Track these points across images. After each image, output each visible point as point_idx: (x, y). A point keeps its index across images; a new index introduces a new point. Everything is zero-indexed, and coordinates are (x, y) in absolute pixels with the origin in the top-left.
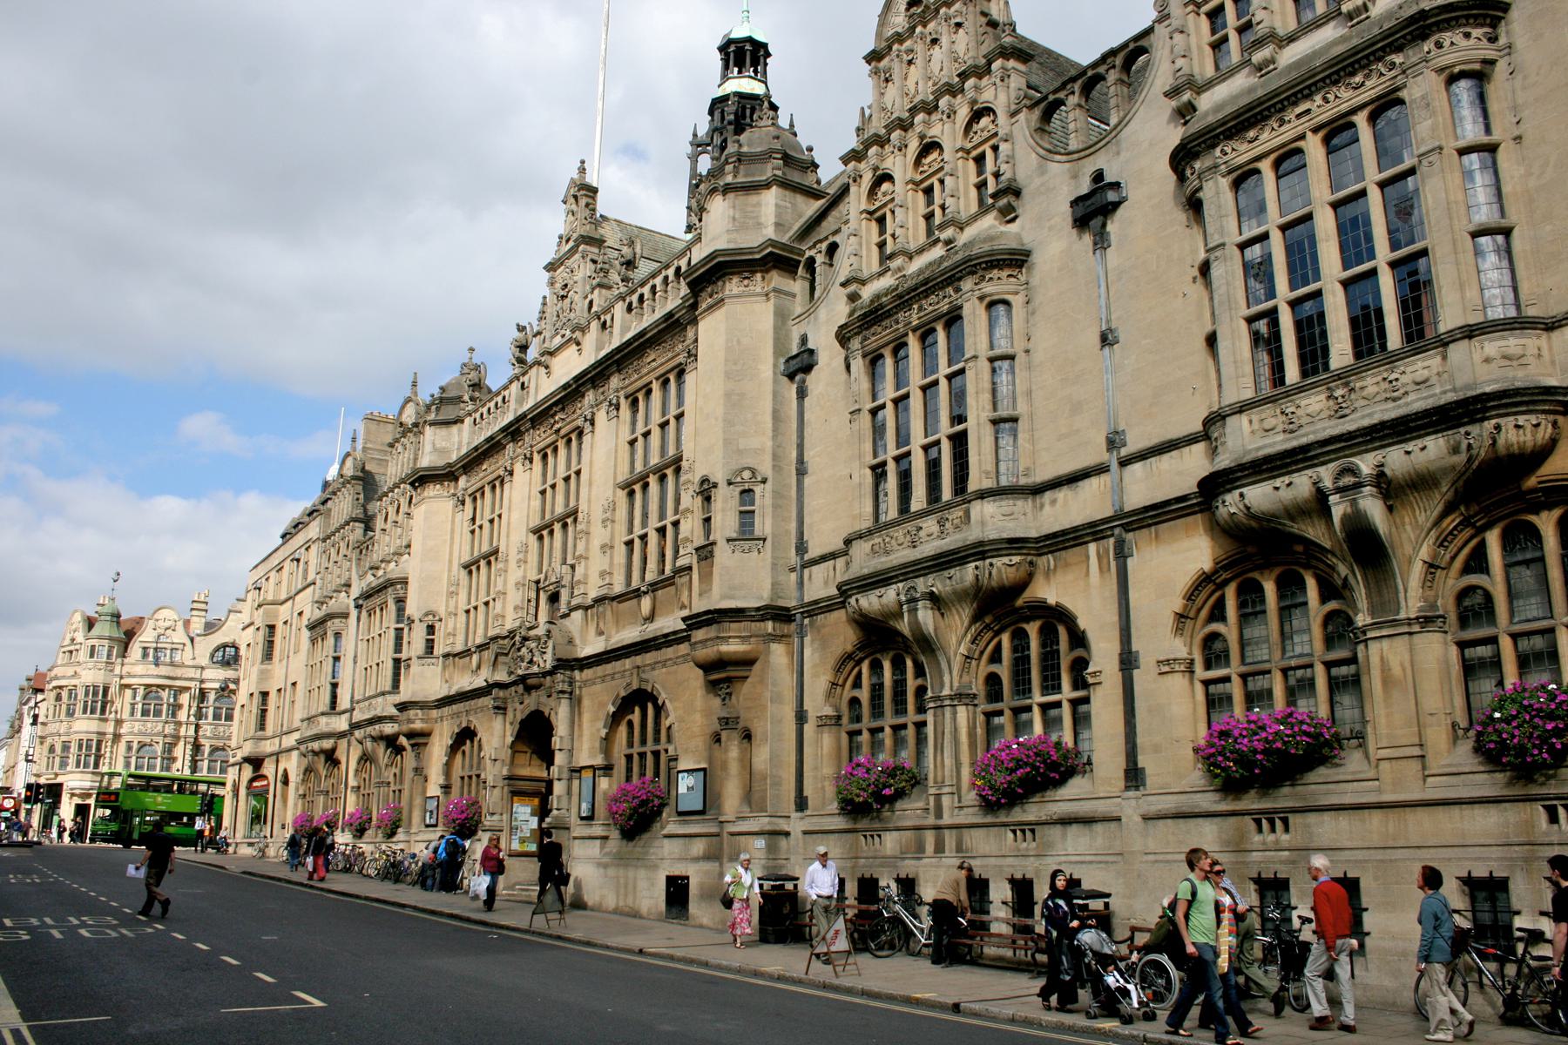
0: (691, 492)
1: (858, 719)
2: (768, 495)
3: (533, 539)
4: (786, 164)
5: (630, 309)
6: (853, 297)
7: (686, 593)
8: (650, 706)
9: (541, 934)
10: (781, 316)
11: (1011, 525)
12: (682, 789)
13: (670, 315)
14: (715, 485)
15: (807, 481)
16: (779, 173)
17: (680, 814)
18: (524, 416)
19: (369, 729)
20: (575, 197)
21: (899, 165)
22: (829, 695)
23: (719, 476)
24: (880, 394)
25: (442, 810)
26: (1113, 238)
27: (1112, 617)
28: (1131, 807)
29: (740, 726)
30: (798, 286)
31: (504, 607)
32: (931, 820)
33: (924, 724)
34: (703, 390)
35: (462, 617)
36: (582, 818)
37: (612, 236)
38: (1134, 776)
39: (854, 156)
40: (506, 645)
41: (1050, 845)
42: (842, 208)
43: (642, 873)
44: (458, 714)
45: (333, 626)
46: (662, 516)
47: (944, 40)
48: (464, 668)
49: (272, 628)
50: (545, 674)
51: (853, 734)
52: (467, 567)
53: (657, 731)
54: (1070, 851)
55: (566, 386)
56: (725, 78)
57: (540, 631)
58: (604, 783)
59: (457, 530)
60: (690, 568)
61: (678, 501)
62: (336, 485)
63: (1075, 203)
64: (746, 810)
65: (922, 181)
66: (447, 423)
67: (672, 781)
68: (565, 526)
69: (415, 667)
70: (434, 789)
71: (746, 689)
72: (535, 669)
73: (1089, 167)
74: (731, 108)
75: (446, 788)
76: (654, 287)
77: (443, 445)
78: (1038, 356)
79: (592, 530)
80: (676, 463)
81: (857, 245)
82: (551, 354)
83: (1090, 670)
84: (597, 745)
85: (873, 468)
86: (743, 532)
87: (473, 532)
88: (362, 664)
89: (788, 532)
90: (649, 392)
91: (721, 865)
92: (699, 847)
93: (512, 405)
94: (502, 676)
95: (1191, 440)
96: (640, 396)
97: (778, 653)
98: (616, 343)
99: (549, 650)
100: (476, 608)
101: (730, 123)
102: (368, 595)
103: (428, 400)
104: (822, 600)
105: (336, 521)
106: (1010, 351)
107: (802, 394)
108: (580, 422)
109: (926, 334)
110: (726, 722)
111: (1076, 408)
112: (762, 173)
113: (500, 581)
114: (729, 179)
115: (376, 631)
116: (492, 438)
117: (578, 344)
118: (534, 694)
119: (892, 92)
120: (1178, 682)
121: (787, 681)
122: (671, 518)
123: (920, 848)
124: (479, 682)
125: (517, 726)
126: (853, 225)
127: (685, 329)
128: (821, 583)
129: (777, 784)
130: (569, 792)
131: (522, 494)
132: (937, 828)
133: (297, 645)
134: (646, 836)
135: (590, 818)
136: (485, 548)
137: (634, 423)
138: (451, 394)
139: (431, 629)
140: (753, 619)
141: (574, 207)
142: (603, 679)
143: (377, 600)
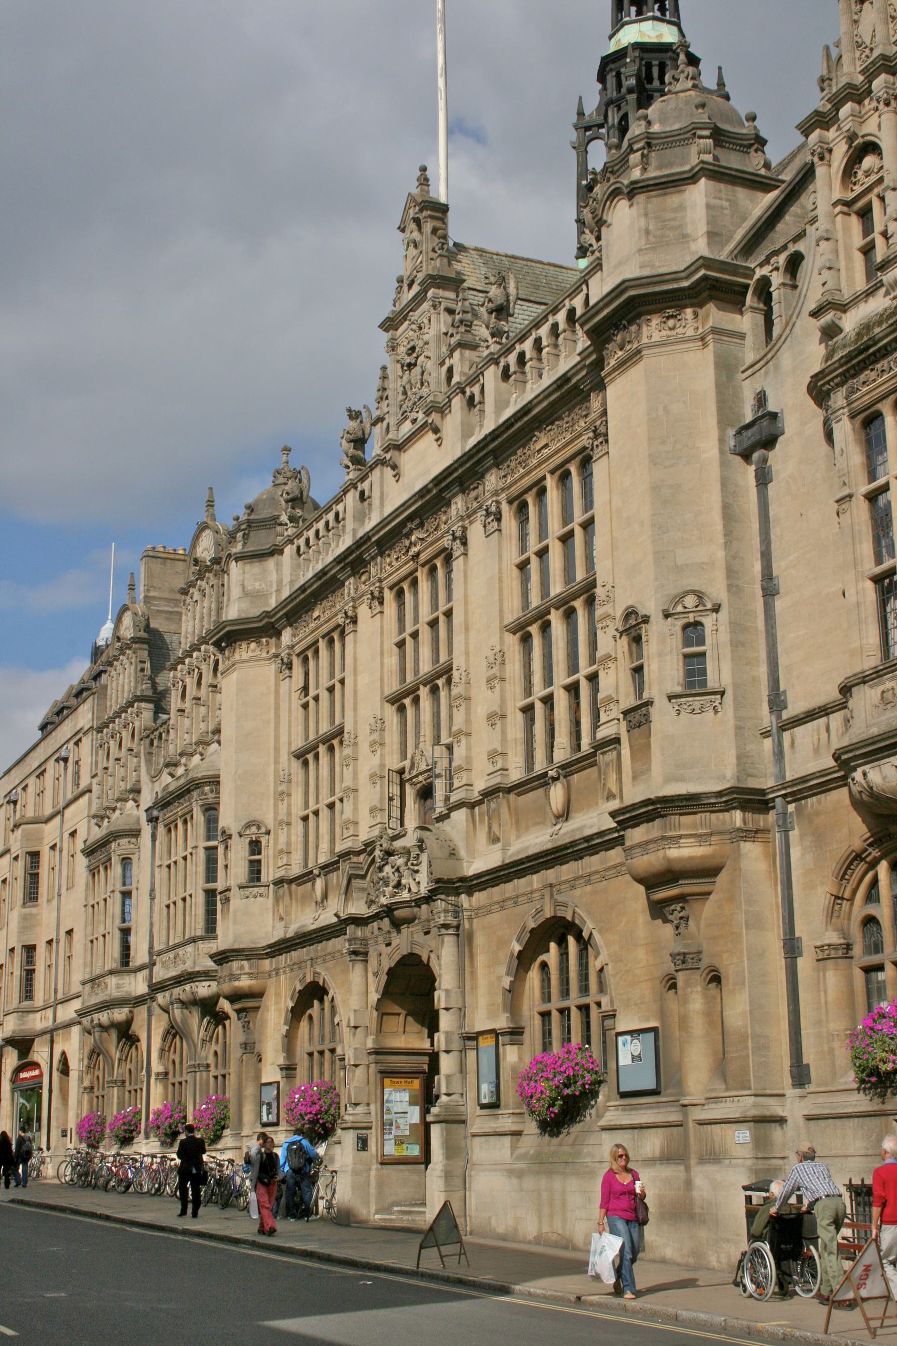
0: (611, 631)
1: (877, 948)
2: (724, 629)
3: (390, 711)
4: (718, 143)
5: (506, 375)
6: (830, 332)
7: (613, 777)
8: (571, 940)
9: (433, 1277)
10: (726, 369)
12: (625, 1059)
13: (564, 379)
14: (646, 620)
15: (779, 604)
16: (708, 158)
17: (624, 1095)
18: (366, 538)
19: (177, 991)
20: (417, 221)
22: (831, 914)
23: (651, 606)
24: (880, 469)
25: (284, 1101)
29: (703, 964)
30: (747, 322)
34: (618, 481)
35: (299, 827)
36: (483, 1107)
37: (472, 272)
39: (821, 120)
40: (359, 863)
42: (806, 200)
43: (573, 1184)
44: (300, 964)
45: (119, 848)
46: (573, 668)
48: (305, 899)
49: (35, 856)
50: (419, 902)
52: (301, 756)
53: (584, 977)
55: (422, 492)
57: (409, 841)
58: (511, 1055)
59: (284, 706)
60: (617, 740)
62: (112, 652)
64: (720, 1089)
66: (260, 556)
67: (609, 1048)
68: (435, 690)
69: (236, 901)
70: (271, 1073)
71: (708, 909)
72: (405, 895)
74: (630, 69)
75: (289, 1069)
76: (538, 341)
79: (474, 693)
80: (589, 591)
81: (832, 252)
82: (400, 447)
84: (499, 1000)
85: (877, 580)
86: (690, 685)
87: (305, 706)
88: (162, 900)
89: (755, 680)
90: (542, 492)
91: (688, 1169)
93: (349, 524)
94: (358, 908)
96: (530, 499)
97: (751, 850)
98: (489, 426)
99: (424, 868)
100: (316, 813)
101: (630, 91)
102: (164, 803)
103: (231, 524)
104: (812, 776)
105: (115, 700)
107: (763, 479)
108: (446, 542)
110: (684, 960)
112: (684, 160)
113: (348, 773)
114: (636, 174)
115: (178, 853)
116: (323, 573)
117: (436, 430)
118: (404, 929)
121: (769, 897)
122: (585, 669)
124: (327, 918)
126: (823, 224)
127: (587, 398)
128: (809, 751)
129: (763, 1046)
130: (462, 1069)
131: (371, 652)
133: (71, 878)
134: (576, 1128)
135: (495, 1105)
136: (325, 728)
137: (523, 537)
138: (264, 513)
139: (255, 846)
140: (713, 809)
141: (416, 235)
142: (502, 904)
143: (177, 809)
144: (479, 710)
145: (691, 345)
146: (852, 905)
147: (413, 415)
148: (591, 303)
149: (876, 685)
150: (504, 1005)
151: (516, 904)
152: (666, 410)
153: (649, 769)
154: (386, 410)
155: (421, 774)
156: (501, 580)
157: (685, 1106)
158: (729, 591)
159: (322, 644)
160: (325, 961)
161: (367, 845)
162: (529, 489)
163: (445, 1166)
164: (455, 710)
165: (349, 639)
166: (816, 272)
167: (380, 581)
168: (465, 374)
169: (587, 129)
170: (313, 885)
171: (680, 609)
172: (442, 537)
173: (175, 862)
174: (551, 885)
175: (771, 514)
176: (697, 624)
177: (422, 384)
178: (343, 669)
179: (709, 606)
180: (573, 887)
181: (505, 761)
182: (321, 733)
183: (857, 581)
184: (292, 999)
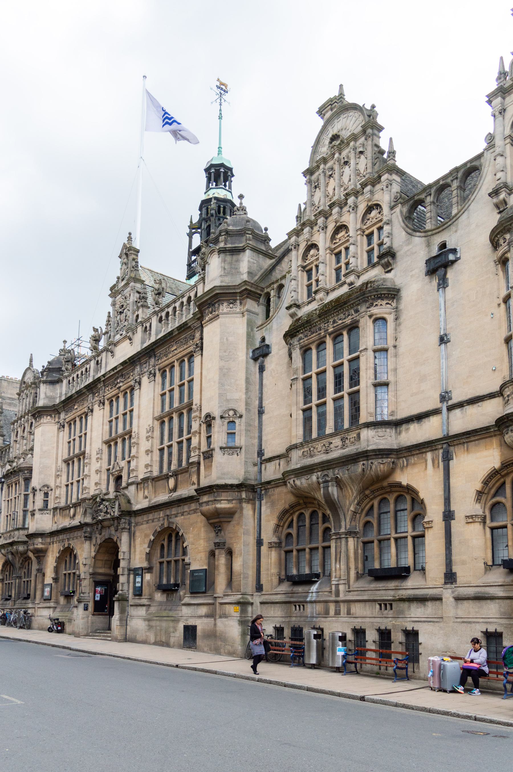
5: (160, 320)
10: (250, 324)
11: (383, 442)
14: (214, 418)
15: (264, 417)
18: (99, 379)
20: (126, 254)
21: (322, 240)
23: (217, 414)
26: (450, 282)
27: (440, 492)
28: (448, 595)
31: (89, 483)
32: (333, 598)
33: (329, 547)
35: (64, 489)
38: (450, 577)
40: (96, 502)
41: (402, 612)
47: (352, 162)
51: (288, 552)
54: (412, 615)
56: (208, 188)
57: (111, 496)
58: (148, 577)
59: (61, 441)
61: (190, 427)
63: (428, 262)
65: (335, 249)
70: (48, 580)
72: (109, 516)
73: (437, 240)
75: (56, 580)
77: (47, 395)
78: (401, 349)
83: (425, 520)
84: (144, 556)
85: (304, 411)
91: (215, 620)
92: (203, 610)
93: (92, 373)
94: (88, 520)
95: (491, 396)
98: (153, 339)
106: (385, 346)
107: (262, 369)
108: (132, 383)
109: (337, 337)
111: (423, 378)
114: (222, 245)
117: (130, 339)
119: (319, 194)
120: (477, 527)
123: (327, 612)
124: (76, 522)
125: (98, 547)
129: (246, 577)
130: (128, 582)
131: (98, 424)
132: (337, 602)
137: (163, 384)
139: (46, 495)
144: (142, 448)
145: (238, 315)
146: (283, 528)
147: (121, 332)
148: (198, 296)
149: (301, 449)
150: (146, 558)
151: (153, 521)
152: (227, 339)
153: (211, 474)
154: (109, 329)
155: (117, 471)
156: (154, 400)
157: (216, 597)
158: (246, 410)
159: (78, 419)
160: (73, 539)
161: (93, 496)
162: (168, 365)
163: (120, 617)
164: (132, 448)
165: (89, 418)
166: (289, 292)
167: (104, 396)
168: (144, 318)
169: (193, 229)
170: (70, 511)
171: (227, 415)
172: (131, 381)
173: (11, 500)
174: (168, 516)
175: (264, 383)
176: (233, 422)
177: (125, 320)
178: (86, 429)
179: (238, 416)
180: (176, 517)
181: (152, 468)
182: (75, 453)
183: (297, 410)
184: (59, 553)
